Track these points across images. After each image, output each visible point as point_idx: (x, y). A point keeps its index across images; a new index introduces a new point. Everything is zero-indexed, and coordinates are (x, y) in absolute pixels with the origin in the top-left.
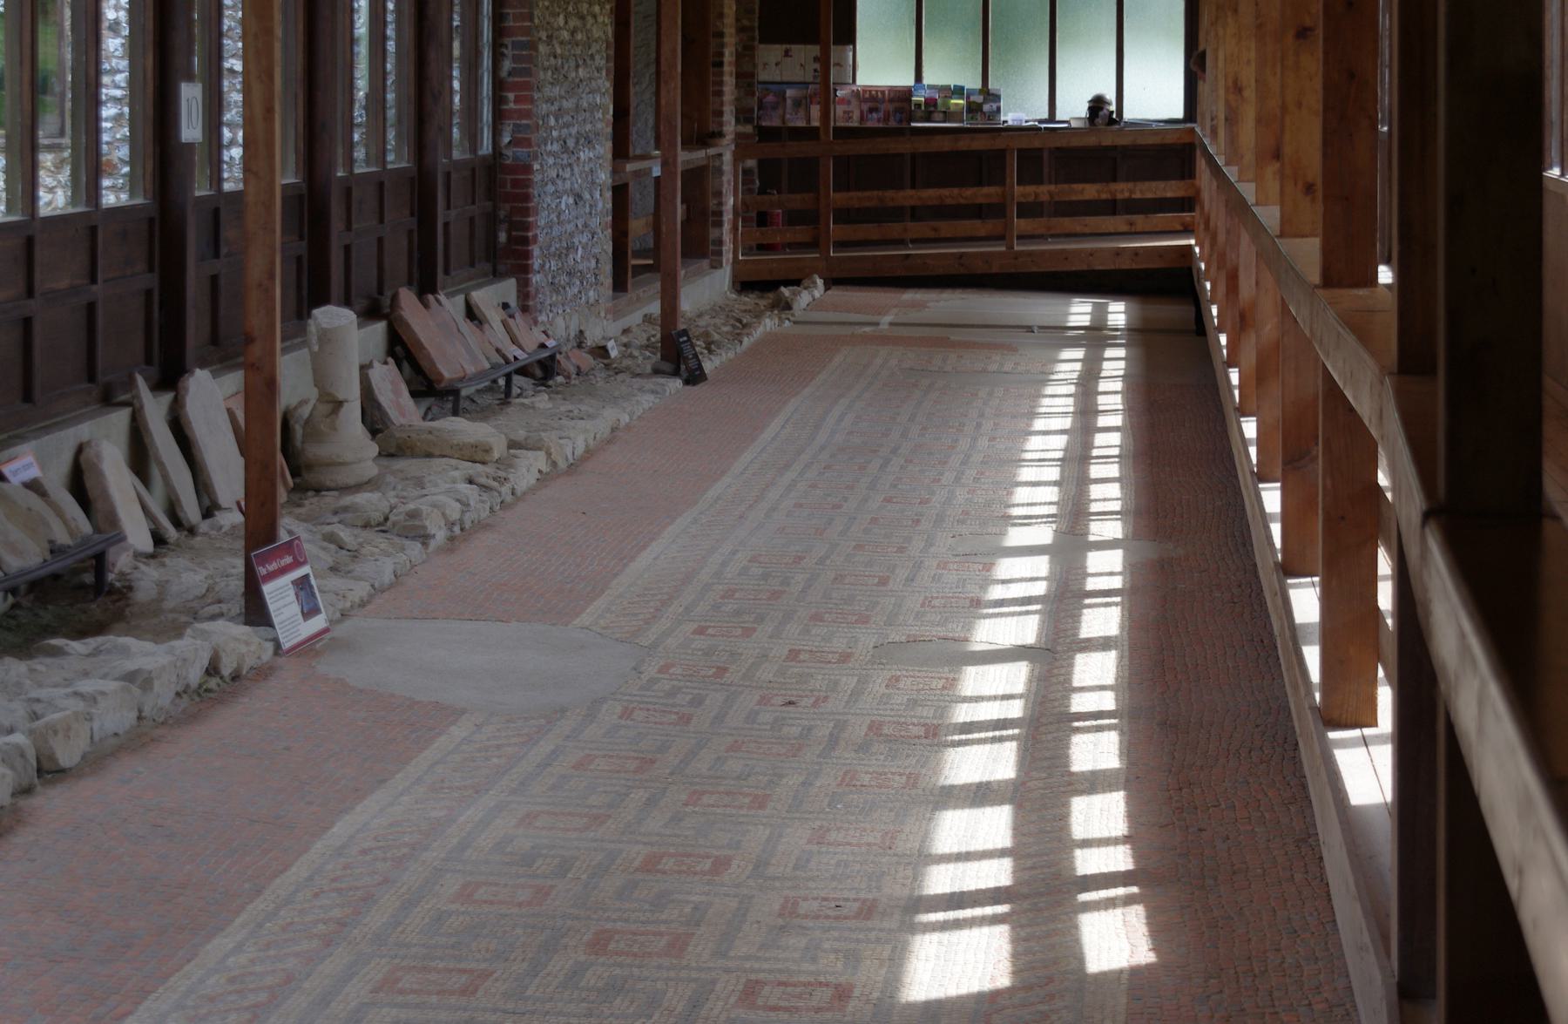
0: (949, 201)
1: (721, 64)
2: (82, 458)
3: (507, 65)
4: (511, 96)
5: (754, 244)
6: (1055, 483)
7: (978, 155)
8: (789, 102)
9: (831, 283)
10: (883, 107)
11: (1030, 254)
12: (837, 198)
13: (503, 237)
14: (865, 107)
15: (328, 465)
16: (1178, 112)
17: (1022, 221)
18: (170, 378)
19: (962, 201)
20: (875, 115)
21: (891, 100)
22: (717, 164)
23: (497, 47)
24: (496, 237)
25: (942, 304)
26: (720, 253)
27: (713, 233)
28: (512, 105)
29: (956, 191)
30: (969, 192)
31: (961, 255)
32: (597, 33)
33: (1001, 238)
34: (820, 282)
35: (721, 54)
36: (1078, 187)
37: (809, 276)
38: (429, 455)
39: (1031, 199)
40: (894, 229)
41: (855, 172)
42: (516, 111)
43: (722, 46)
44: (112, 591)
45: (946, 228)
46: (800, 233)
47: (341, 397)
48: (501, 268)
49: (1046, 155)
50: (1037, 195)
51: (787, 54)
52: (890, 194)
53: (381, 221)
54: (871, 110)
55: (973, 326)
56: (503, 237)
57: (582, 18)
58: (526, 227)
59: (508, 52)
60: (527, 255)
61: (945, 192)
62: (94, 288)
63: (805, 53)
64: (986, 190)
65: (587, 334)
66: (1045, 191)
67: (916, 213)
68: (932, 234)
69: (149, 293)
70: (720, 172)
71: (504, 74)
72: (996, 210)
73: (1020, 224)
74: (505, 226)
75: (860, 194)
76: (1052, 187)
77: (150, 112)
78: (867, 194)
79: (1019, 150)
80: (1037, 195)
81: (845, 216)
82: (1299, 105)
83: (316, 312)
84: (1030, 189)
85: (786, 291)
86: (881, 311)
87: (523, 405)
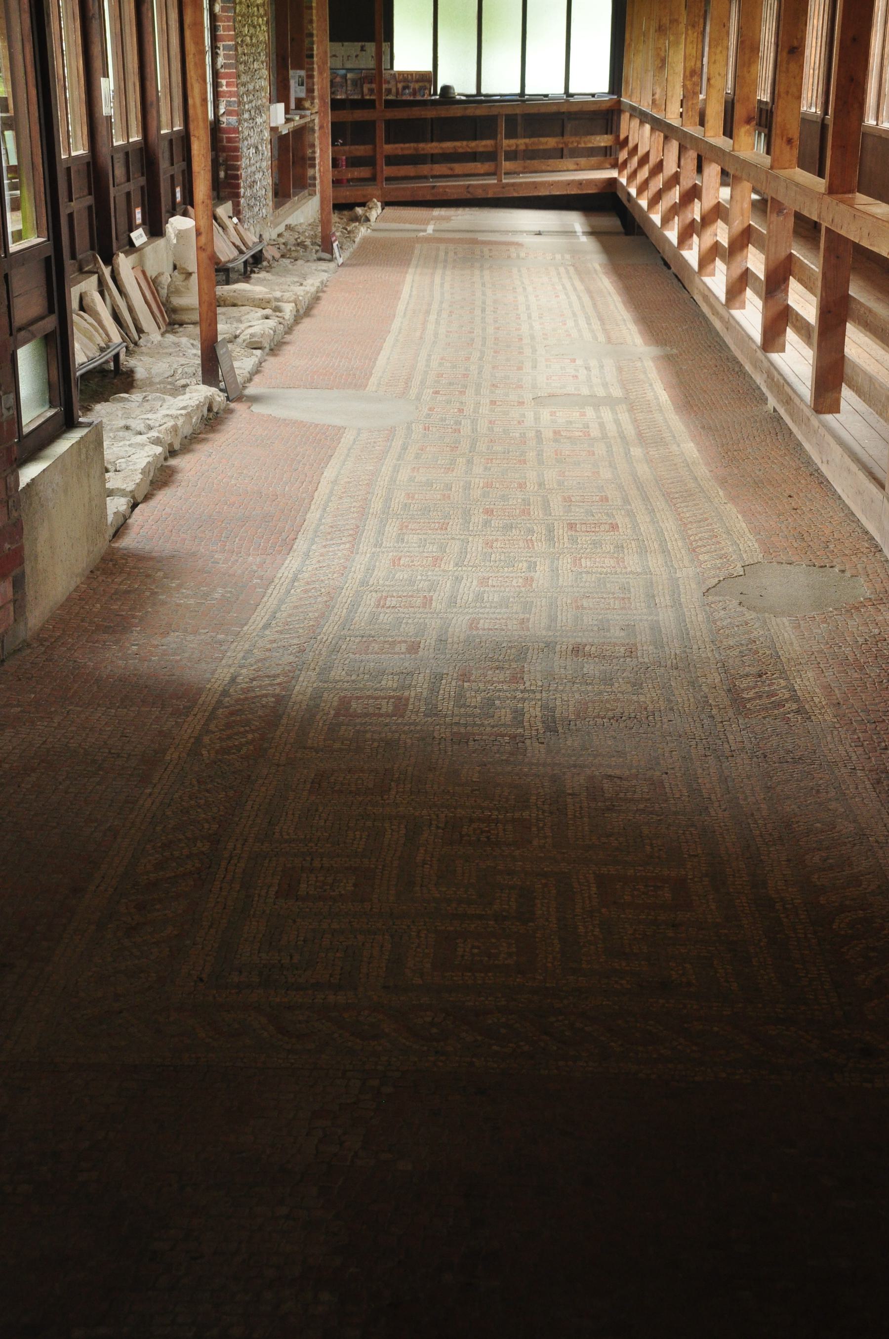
0: (460, 150)
1: (312, 56)
2: (84, 303)
3: (221, 61)
4: (224, 82)
5: (789, 147)
6: (110, 493)
7: (474, 119)
8: (349, 82)
9: (386, 204)
10: (412, 85)
11: (513, 185)
12: (389, 149)
13: (222, 174)
14: (400, 86)
15: (186, 310)
16: (605, 88)
17: (507, 163)
18: (109, 260)
19: (469, 150)
20: (407, 91)
21: (417, 81)
22: (311, 125)
23: (214, 48)
24: (218, 175)
25: (459, 217)
26: (314, 185)
27: (310, 172)
28: (224, 88)
29: (465, 143)
30: (473, 144)
31: (469, 186)
32: (261, 38)
33: (494, 174)
34: (379, 204)
35: (312, 49)
36: (543, 140)
37: (370, 200)
38: (234, 305)
39: (514, 148)
40: (425, 169)
41: (400, 131)
42: (227, 92)
43: (312, 43)
44: (123, 373)
45: (458, 168)
46: (363, 172)
47: (190, 271)
48: (222, 194)
49: (519, 118)
50: (517, 146)
51: (362, 49)
52: (421, 145)
53: (172, 164)
54: (404, 88)
55: (491, 232)
56: (222, 174)
57: (254, 27)
58: (237, 168)
59: (221, 52)
60: (238, 186)
61: (458, 144)
62: (72, 204)
63: (371, 47)
64: (484, 142)
65: (264, 237)
66: (521, 143)
67: (434, 159)
68: (449, 172)
69: (90, 208)
70: (313, 131)
71: (219, 66)
72: (491, 156)
73: (506, 165)
74: (222, 168)
75: (402, 145)
76: (527, 140)
77: (83, 96)
78: (407, 145)
79: (506, 115)
80: (517, 146)
81: (392, 160)
82: (787, 93)
83: (170, 219)
84: (512, 142)
85: (359, 211)
86: (427, 222)
87: (259, 278)
